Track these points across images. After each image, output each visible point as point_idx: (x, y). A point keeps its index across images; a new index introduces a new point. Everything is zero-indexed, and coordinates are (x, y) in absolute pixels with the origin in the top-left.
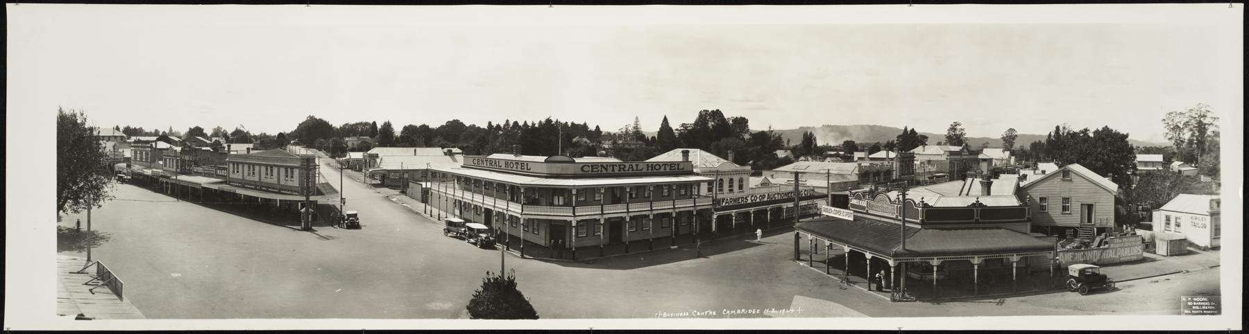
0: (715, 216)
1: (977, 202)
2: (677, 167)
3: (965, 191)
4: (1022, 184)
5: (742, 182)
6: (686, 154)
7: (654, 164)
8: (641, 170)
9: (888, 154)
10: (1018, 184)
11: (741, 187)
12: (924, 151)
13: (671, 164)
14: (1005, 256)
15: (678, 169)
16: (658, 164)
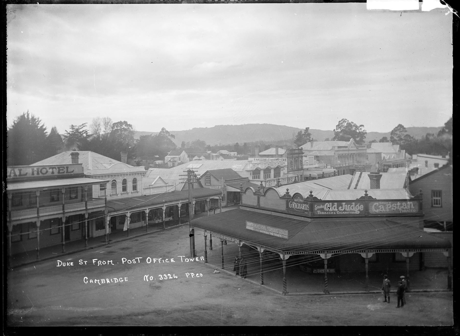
0: (108, 219)
1: (366, 195)
2: (65, 170)
3: (353, 185)
4: (413, 178)
5: (136, 183)
6: (75, 156)
7: (40, 168)
8: (73, 172)
9: (277, 151)
10: (410, 178)
11: (135, 188)
12: (312, 146)
13: (60, 167)
14: (397, 251)
15: (67, 172)
16: (44, 167)
